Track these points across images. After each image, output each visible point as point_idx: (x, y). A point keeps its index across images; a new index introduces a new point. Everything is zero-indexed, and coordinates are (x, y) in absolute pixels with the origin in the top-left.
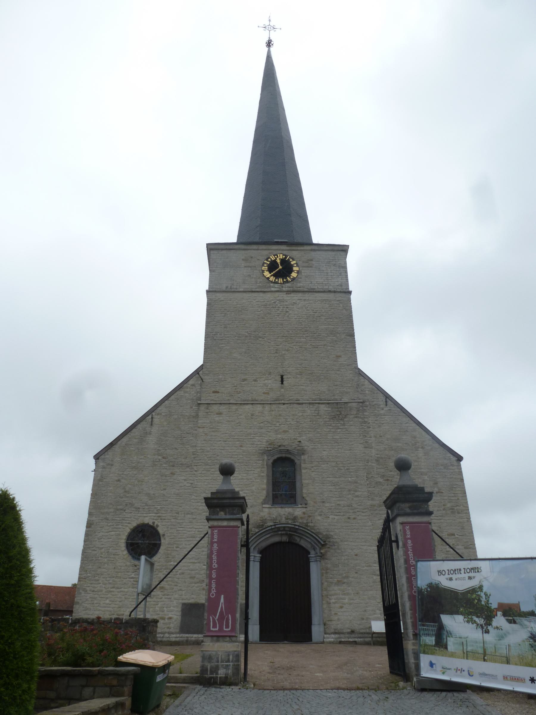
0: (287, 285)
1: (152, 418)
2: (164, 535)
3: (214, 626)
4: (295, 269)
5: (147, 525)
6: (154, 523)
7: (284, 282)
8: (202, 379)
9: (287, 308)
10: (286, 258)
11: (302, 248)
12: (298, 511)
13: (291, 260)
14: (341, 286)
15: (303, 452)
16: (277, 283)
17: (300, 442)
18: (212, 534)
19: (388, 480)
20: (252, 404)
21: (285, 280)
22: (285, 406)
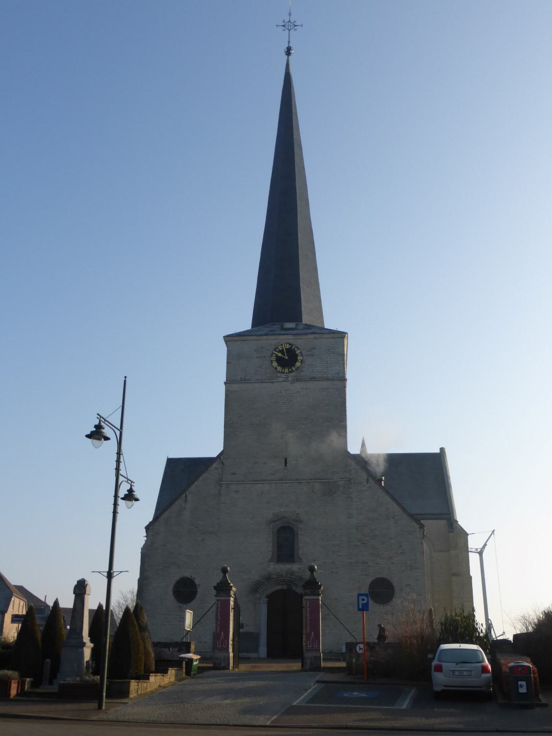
0: (292, 374)
1: (186, 496)
2: (199, 585)
3: (310, 645)
4: (300, 358)
5: (187, 578)
6: (191, 576)
7: (289, 371)
8: (223, 463)
9: (291, 396)
10: (292, 347)
11: (306, 337)
12: (295, 567)
13: (296, 349)
14: (338, 374)
15: (300, 521)
16: (283, 373)
17: (298, 514)
18: (218, 604)
19: (363, 543)
20: (262, 483)
21: (290, 370)
22: (288, 484)
